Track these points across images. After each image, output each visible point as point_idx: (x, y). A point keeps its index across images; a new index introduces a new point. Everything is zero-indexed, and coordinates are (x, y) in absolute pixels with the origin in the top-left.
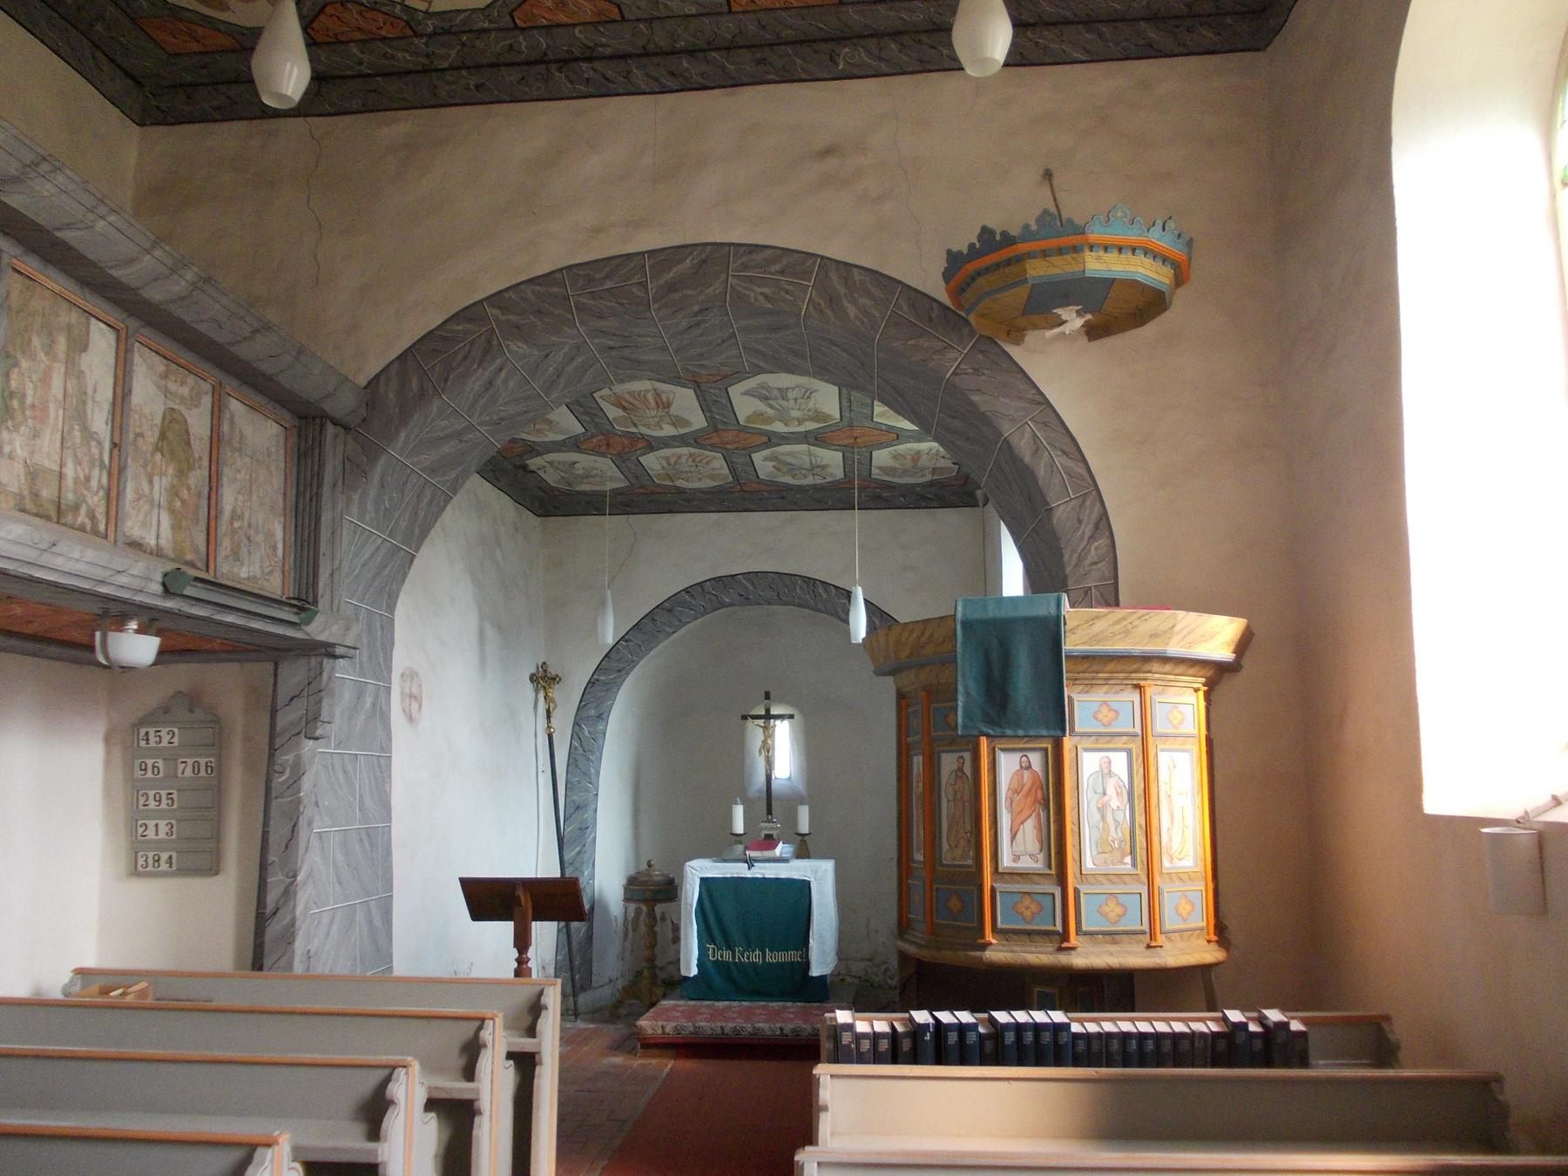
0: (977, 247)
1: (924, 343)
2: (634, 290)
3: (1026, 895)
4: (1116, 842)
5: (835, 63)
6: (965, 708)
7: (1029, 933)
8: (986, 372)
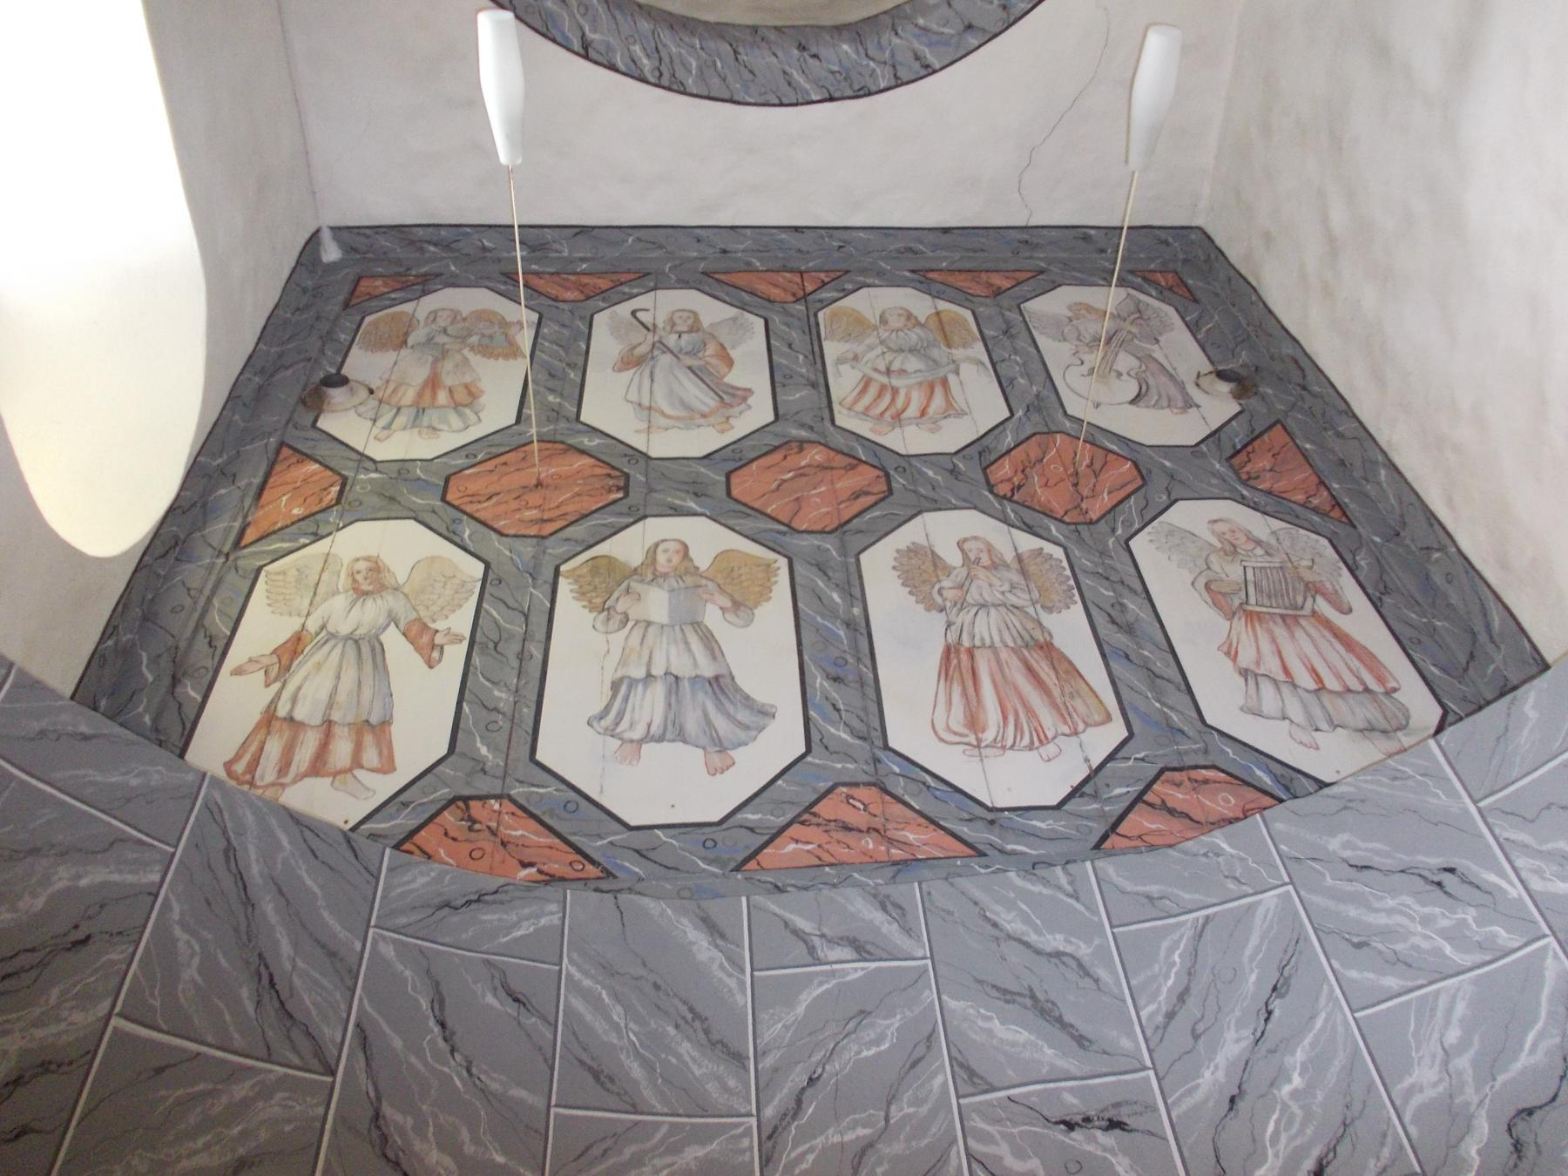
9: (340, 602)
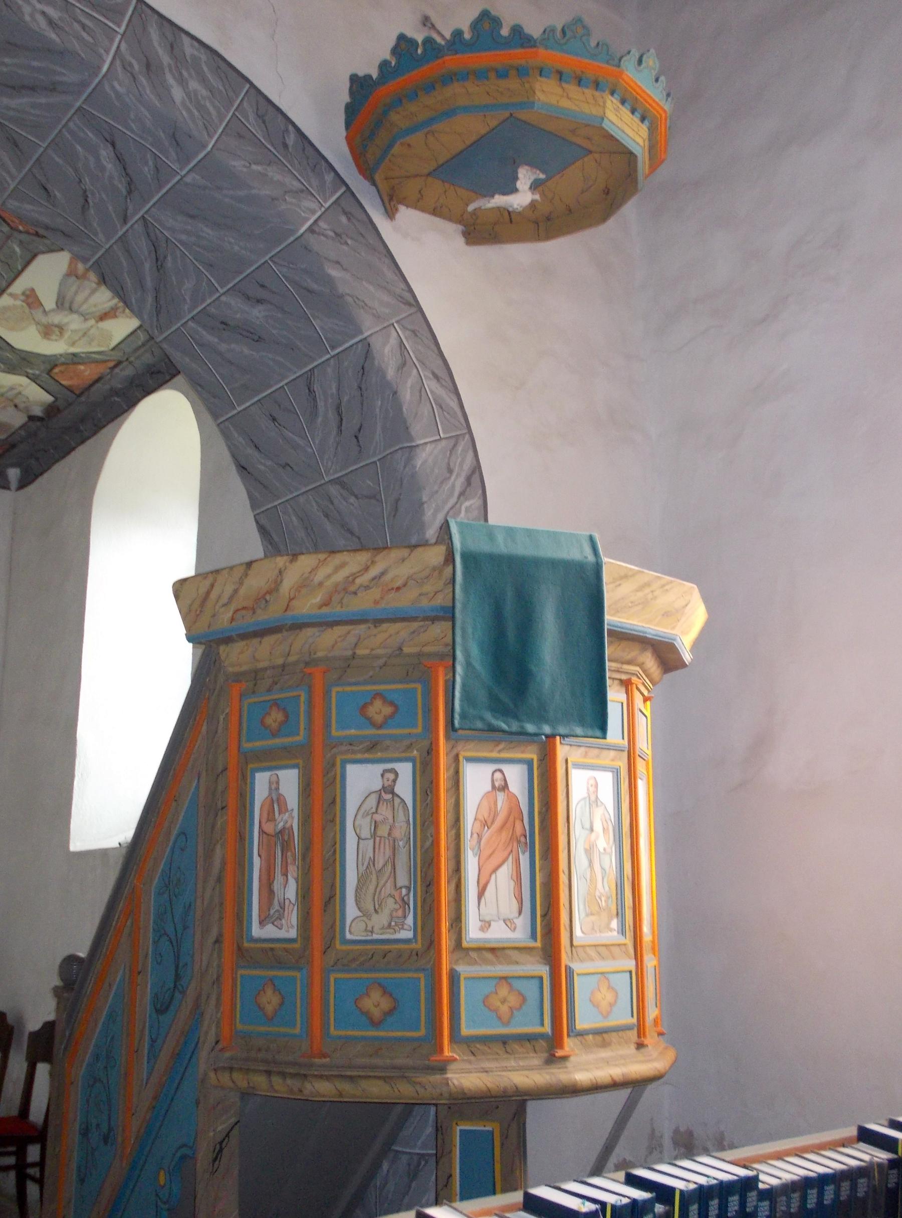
0: (393, 64)
1: (274, 173)
3: (503, 981)
4: (603, 899)
6: (464, 685)
7: (504, 1041)
8: (349, 242)
9: (74, 326)
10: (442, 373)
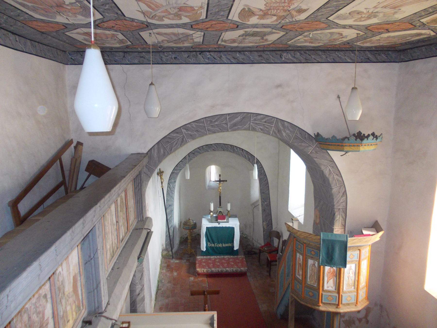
1: (303, 144)
2: (224, 125)
5: (282, 58)
7: (330, 304)
10: (338, 174)
